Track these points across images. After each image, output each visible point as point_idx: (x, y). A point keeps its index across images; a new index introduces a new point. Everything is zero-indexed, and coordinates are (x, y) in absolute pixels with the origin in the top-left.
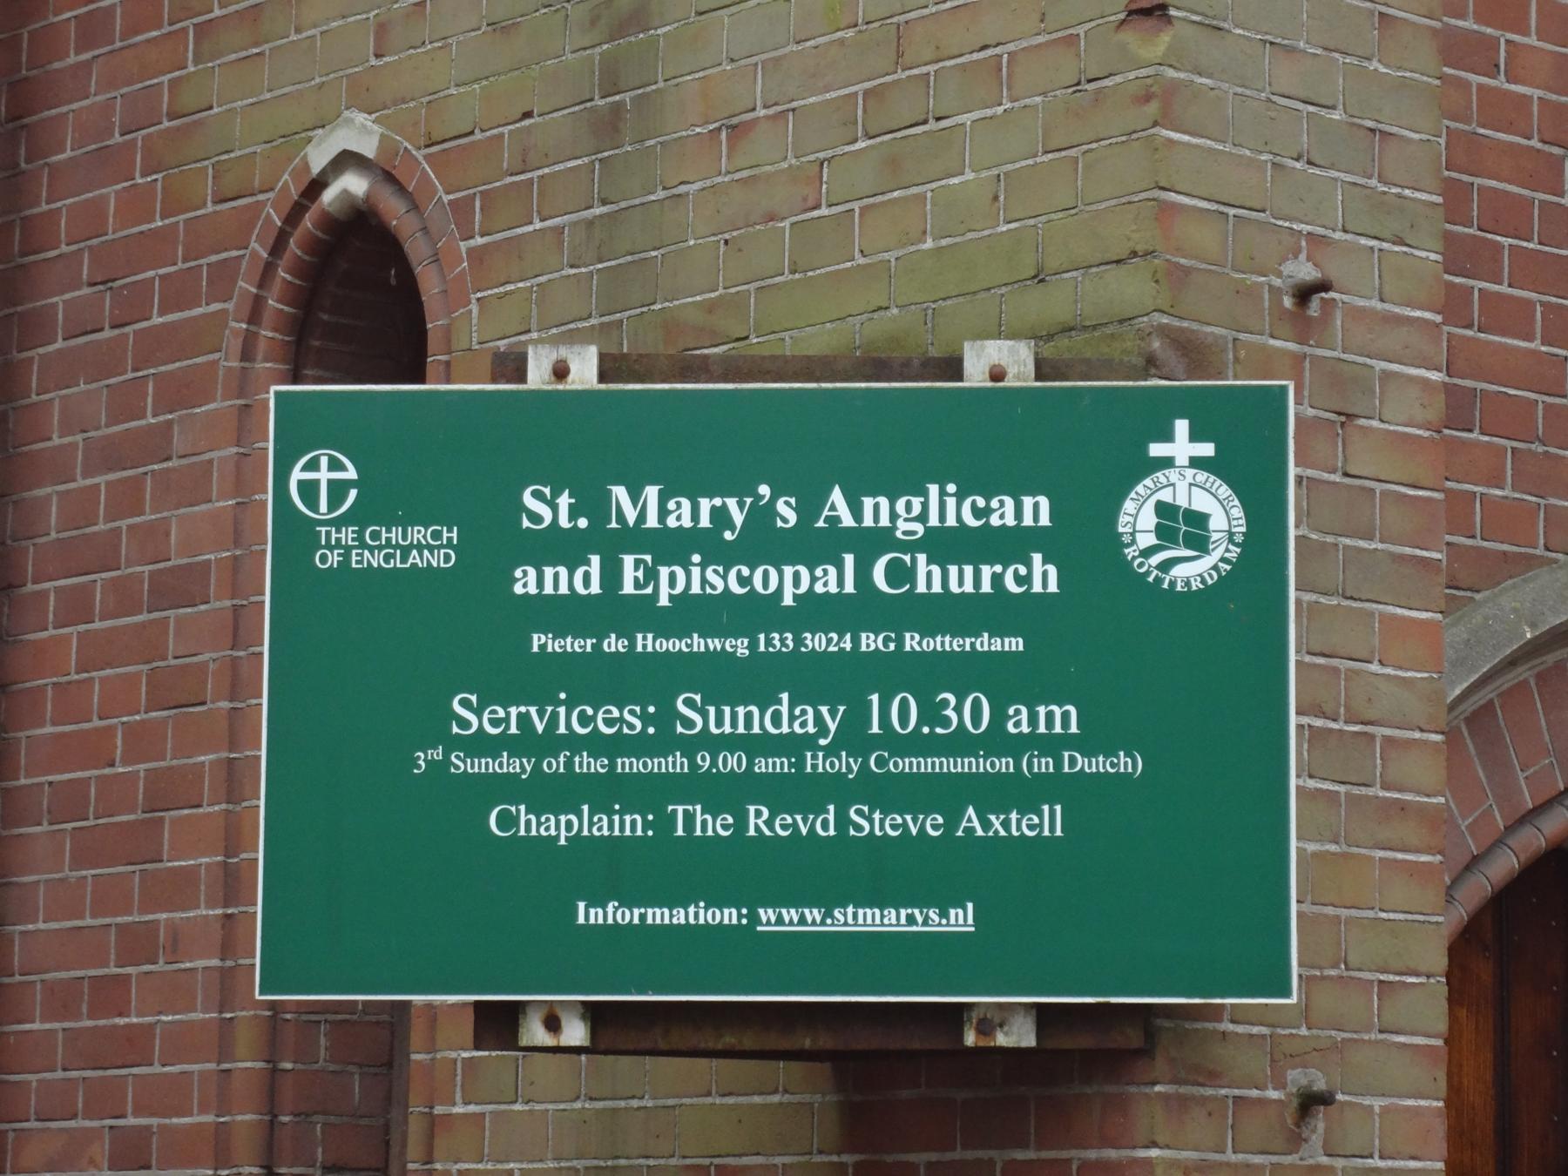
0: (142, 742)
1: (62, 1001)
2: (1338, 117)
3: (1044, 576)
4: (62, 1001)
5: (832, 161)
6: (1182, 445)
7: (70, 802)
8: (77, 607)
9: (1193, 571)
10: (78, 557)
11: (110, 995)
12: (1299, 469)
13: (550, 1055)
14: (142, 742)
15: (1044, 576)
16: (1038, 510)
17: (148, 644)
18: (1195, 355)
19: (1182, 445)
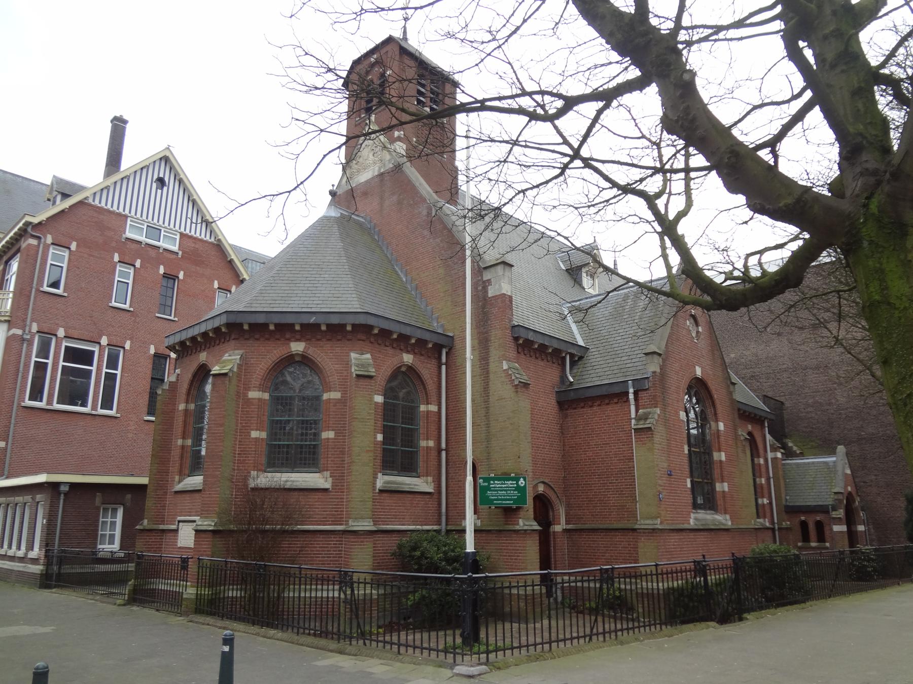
0: (458, 490)
1: (452, 504)
2: (828, 260)
3: (515, 485)
4: (452, 504)
5: (523, 38)
6: (522, 479)
7: (452, 493)
8: (452, 482)
9: (522, 485)
10: (452, 479)
11: (456, 504)
12: (773, 453)
13: (637, 140)
14: (458, 490)
15: (515, 485)
16: (515, 482)
17: (458, 484)
18: (522, 475)
19: (522, 479)
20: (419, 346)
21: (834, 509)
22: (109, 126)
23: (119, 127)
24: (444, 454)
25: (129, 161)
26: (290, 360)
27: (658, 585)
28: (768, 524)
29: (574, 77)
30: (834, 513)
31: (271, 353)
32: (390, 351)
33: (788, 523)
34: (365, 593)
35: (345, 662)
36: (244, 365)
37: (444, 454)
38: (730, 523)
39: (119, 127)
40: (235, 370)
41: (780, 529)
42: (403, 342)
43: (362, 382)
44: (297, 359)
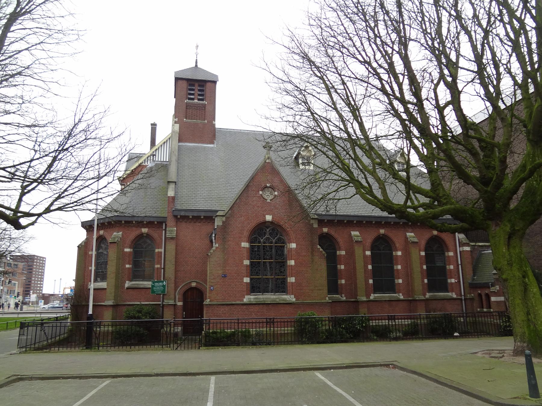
20: (150, 224)
21: (493, 285)
22: (150, 127)
23: (154, 127)
24: (460, 266)
25: (158, 141)
26: (141, 236)
27: (170, 330)
28: (455, 296)
29: (278, 80)
30: (493, 288)
31: (133, 234)
32: (134, 228)
33: (473, 295)
34: (27, 338)
35: (123, 372)
36: (123, 238)
37: (460, 266)
38: (294, 300)
39: (154, 127)
40: (119, 240)
41: (465, 299)
42: (140, 224)
43: (112, 245)
44: (145, 235)
